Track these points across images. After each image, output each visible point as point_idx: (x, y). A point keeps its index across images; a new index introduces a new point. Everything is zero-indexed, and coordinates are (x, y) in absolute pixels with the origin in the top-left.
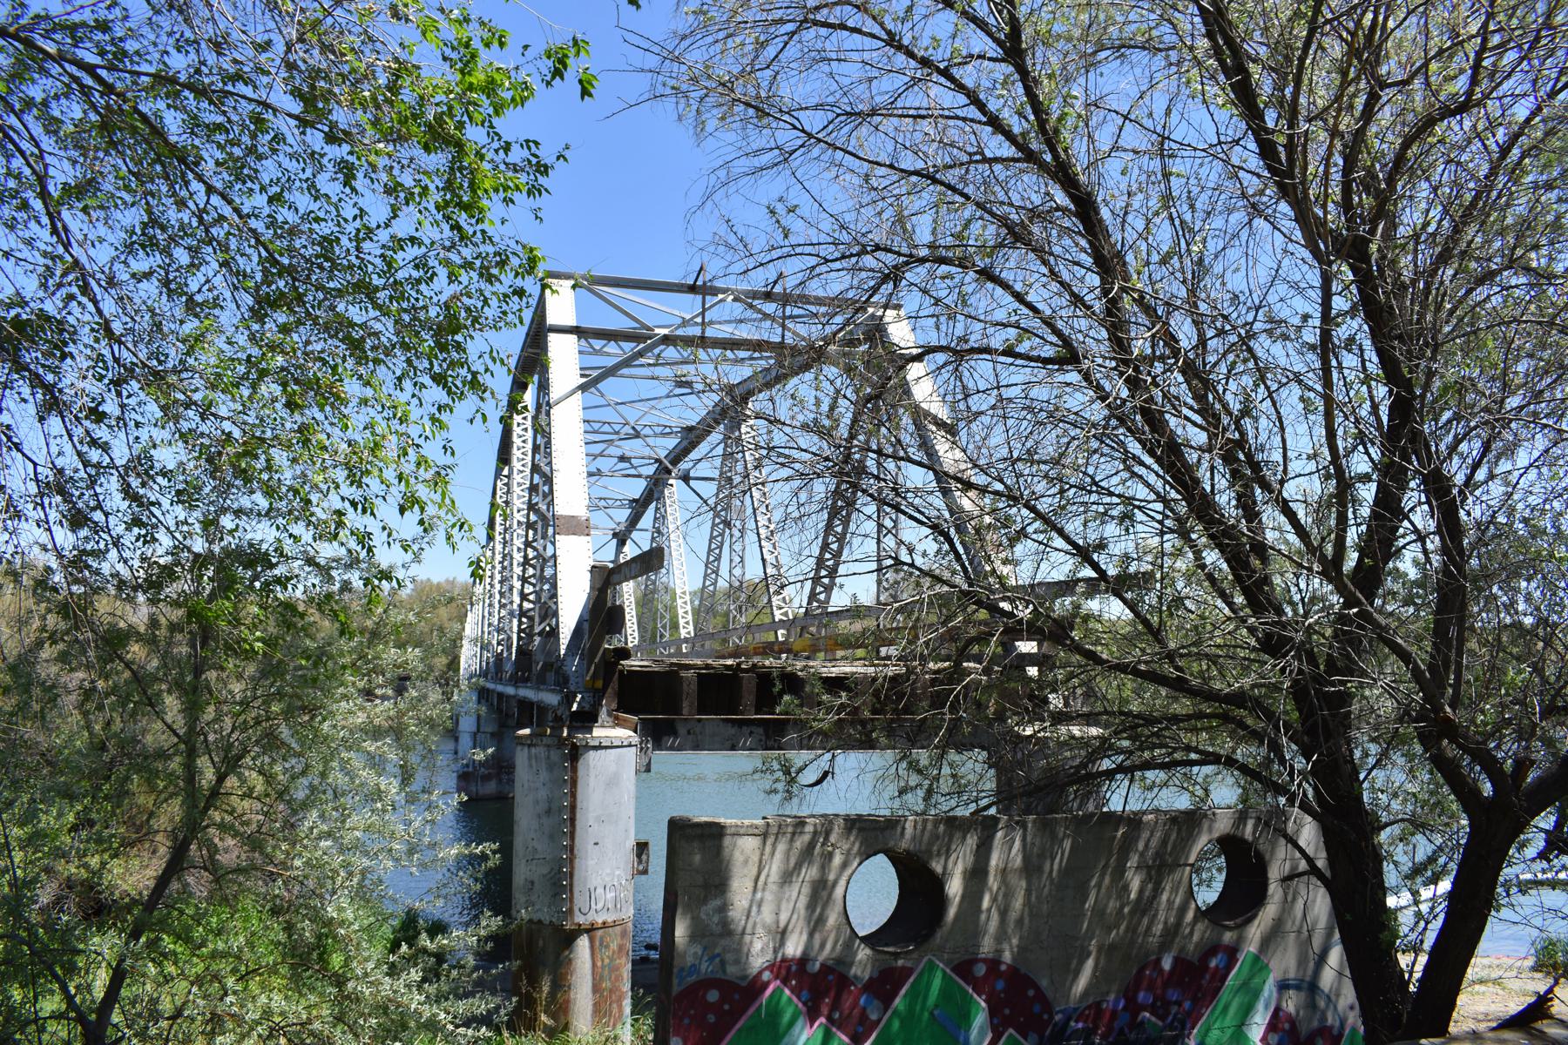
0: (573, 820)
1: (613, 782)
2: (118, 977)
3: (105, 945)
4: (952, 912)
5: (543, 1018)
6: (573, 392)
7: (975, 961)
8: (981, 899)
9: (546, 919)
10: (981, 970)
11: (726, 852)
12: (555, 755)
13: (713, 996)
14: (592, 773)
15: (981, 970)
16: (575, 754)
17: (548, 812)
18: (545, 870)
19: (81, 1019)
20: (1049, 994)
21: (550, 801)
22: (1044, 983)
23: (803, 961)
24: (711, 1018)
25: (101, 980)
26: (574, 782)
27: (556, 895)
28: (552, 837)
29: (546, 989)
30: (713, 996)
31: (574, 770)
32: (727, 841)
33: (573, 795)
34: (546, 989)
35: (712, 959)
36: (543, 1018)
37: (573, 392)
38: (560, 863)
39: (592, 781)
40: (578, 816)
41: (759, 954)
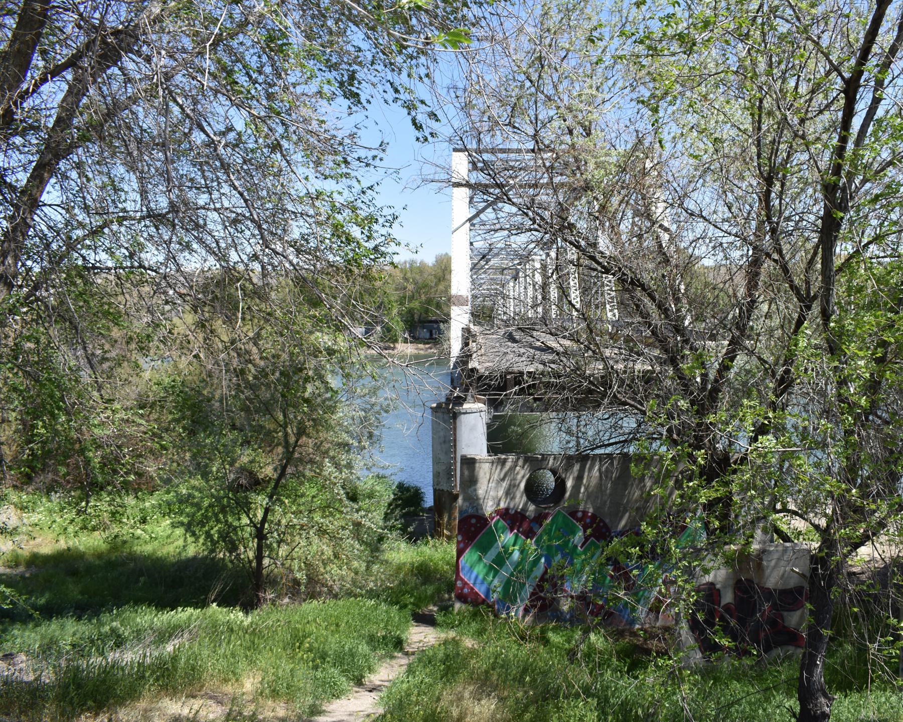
0: (455, 446)
1: (473, 428)
2: (267, 511)
3: (260, 500)
4: (568, 494)
5: (445, 531)
6: (464, 224)
7: (577, 511)
8: (580, 488)
9: (445, 489)
10: (580, 515)
11: (477, 469)
12: (446, 417)
13: (473, 521)
14: (463, 425)
15: (580, 515)
16: (455, 416)
17: (444, 442)
18: (444, 468)
19: (255, 526)
20: (609, 525)
21: (445, 437)
22: (607, 521)
23: (507, 509)
24: (473, 529)
25: (260, 514)
26: (455, 429)
27: (449, 479)
28: (446, 453)
29: (446, 520)
30: (473, 521)
31: (455, 423)
32: (477, 465)
33: (455, 434)
34: (446, 520)
35: (473, 508)
36: (445, 531)
37: (464, 224)
38: (451, 465)
39: (463, 428)
40: (458, 444)
41: (489, 508)
